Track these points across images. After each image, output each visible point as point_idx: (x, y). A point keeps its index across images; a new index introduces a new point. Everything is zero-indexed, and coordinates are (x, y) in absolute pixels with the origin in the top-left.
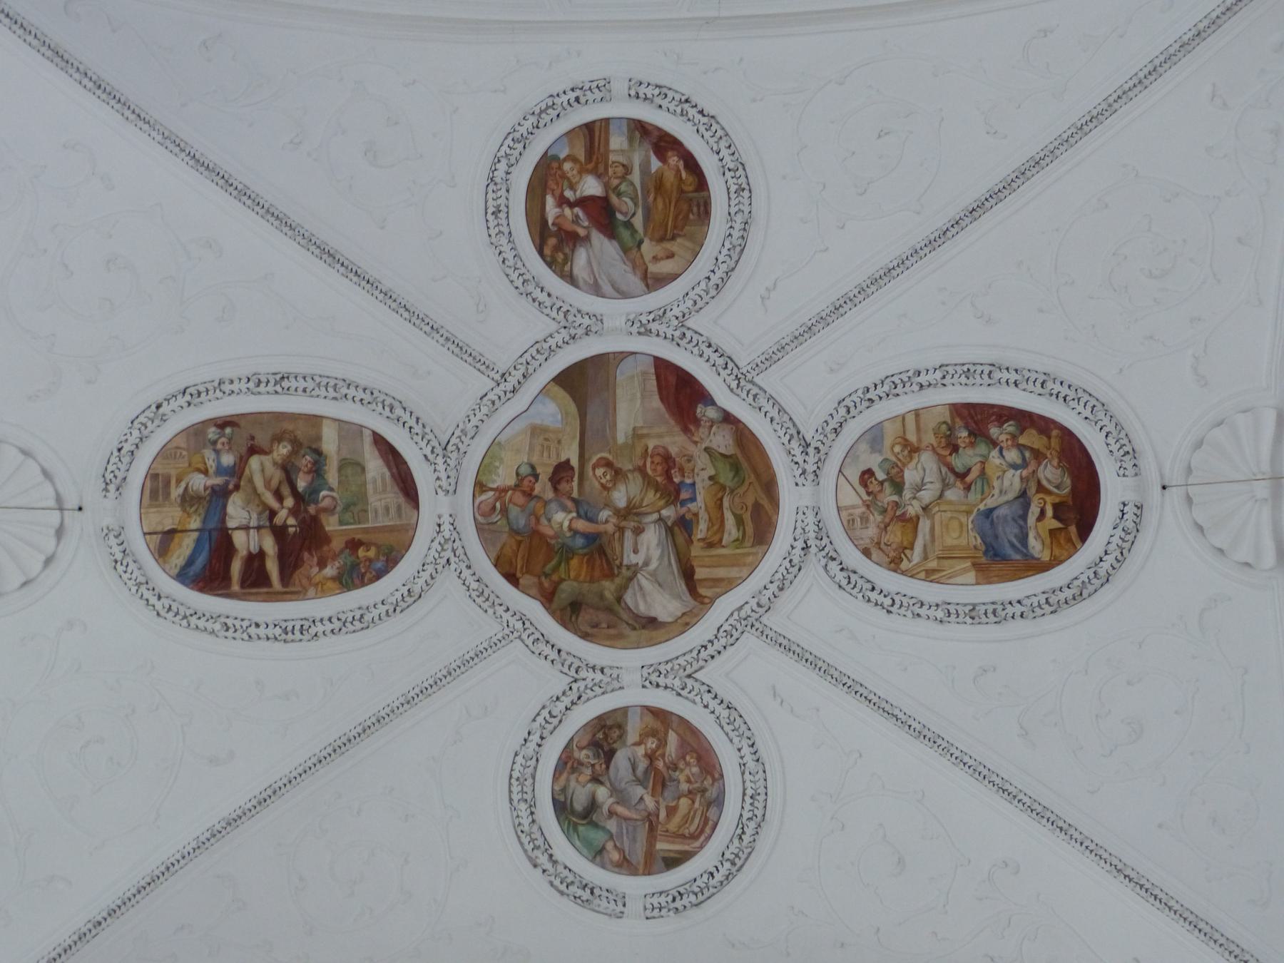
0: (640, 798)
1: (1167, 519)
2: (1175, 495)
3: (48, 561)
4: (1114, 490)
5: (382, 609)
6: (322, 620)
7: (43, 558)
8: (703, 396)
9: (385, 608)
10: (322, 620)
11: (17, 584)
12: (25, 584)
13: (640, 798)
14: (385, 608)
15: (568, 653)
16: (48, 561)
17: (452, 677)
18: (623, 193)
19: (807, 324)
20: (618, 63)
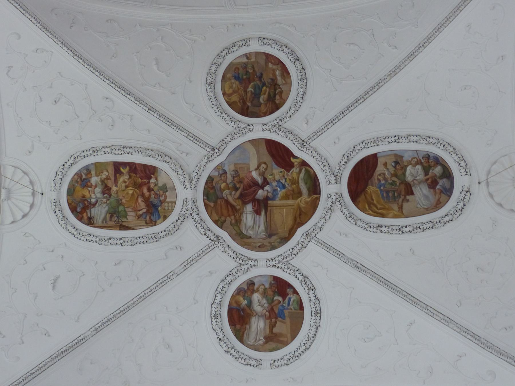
0: (256, 85)
1: (480, 194)
2: (483, 184)
3: (24, 216)
4: (460, 181)
5: (164, 233)
6: (300, 355)
7: (22, 214)
8: (288, 153)
9: (165, 233)
10: (300, 355)
11: (10, 222)
12: (13, 222)
13: (266, 316)
14: (165, 233)
15: (239, 254)
16: (24, 216)
17: (195, 262)
18: (256, 85)
19: (328, 132)
20: (253, 29)
